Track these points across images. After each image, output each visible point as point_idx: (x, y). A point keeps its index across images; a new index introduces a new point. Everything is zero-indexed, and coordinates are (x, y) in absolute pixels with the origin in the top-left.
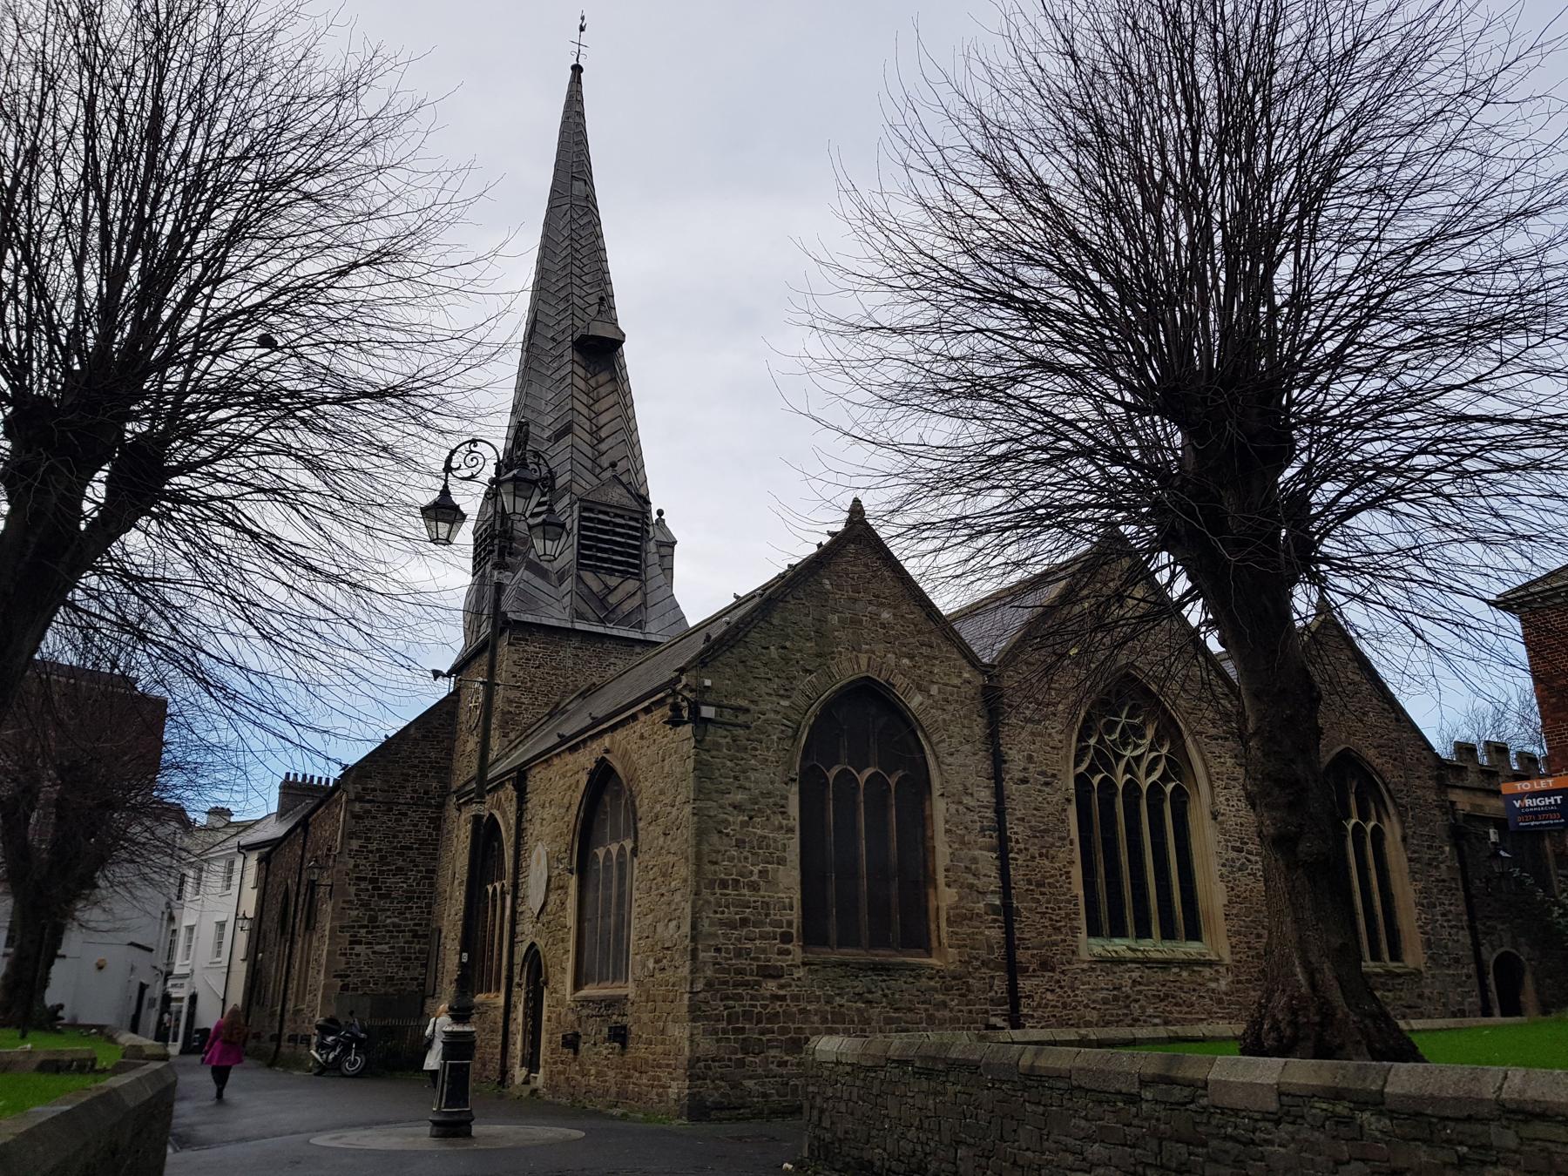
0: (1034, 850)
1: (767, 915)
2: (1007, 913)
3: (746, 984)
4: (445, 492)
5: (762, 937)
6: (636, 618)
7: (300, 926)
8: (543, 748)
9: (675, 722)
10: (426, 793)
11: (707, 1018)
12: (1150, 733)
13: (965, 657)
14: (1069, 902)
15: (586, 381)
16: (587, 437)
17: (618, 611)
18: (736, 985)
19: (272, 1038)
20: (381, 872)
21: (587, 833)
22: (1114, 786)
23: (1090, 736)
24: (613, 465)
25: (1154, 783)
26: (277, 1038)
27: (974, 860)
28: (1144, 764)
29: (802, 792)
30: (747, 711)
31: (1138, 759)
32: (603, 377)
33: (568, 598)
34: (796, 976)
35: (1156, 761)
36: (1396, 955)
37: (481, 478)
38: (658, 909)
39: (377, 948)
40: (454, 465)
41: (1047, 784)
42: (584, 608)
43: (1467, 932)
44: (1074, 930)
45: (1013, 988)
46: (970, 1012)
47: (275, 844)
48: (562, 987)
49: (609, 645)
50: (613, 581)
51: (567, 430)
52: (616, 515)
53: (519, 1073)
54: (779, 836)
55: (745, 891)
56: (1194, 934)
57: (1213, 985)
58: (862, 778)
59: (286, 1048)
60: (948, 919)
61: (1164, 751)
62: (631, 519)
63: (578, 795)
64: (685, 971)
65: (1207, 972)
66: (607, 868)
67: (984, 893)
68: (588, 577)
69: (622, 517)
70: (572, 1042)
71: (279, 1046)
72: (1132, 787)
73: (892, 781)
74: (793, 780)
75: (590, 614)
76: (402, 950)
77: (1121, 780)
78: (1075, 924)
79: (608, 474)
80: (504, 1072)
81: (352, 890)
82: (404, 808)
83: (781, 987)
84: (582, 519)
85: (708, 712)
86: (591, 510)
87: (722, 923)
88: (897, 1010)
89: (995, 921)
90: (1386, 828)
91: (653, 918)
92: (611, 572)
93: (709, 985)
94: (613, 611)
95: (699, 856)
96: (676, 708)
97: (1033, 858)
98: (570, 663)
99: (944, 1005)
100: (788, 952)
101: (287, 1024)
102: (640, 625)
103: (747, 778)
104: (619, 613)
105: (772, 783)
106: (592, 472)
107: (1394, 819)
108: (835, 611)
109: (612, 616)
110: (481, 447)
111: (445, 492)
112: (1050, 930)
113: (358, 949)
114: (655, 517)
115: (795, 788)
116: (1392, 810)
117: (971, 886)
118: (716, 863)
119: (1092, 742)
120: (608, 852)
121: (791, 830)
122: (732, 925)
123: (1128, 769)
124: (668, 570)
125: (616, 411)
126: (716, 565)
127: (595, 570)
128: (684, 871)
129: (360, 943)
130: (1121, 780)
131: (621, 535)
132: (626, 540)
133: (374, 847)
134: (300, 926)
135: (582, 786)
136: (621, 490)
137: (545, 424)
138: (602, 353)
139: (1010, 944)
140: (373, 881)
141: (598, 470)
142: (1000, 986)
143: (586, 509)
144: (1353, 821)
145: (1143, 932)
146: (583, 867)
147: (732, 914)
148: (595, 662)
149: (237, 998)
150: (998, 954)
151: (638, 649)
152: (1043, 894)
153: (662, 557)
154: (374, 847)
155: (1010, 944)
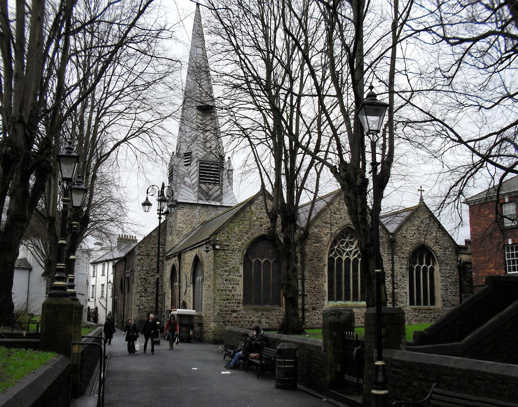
3: (228, 314)
4: (147, 199)
5: (233, 303)
6: (219, 198)
12: (356, 243)
18: (225, 314)
19: (121, 322)
20: (147, 276)
21: (194, 274)
22: (342, 259)
23: (335, 246)
25: (355, 258)
28: (353, 253)
30: (229, 246)
31: (350, 252)
33: (196, 193)
36: (433, 303)
41: (319, 261)
43: (459, 297)
44: (324, 300)
49: (210, 208)
50: (211, 186)
54: (238, 278)
55: (228, 292)
63: (192, 263)
64: (212, 311)
68: (203, 186)
72: (348, 260)
73: (271, 262)
77: (344, 257)
79: (208, 150)
81: (139, 281)
82: (152, 257)
85: (217, 247)
86: (203, 164)
87: (222, 300)
92: (210, 184)
94: (211, 196)
97: (313, 281)
98: (197, 214)
102: (220, 200)
104: (213, 197)
105: (236, 264)
108: (255, 216)
113: (142, 298)
115: (242, 265)
119: (336, 247)
121: (240, 276)
123: (347, 254)
127: (204, 183)
130: (344, 257)
131: (213, 171)
133: (144, 269)
136: (213, 156)
140: (145, 279)
143: (201, 163)
144: (424, 266)
145: (347, 299)
146: (194, 282)
147: (224, 297)
148: (205, 213)
149: (110, 309)
151: (219, 208)
154: (144, 269)
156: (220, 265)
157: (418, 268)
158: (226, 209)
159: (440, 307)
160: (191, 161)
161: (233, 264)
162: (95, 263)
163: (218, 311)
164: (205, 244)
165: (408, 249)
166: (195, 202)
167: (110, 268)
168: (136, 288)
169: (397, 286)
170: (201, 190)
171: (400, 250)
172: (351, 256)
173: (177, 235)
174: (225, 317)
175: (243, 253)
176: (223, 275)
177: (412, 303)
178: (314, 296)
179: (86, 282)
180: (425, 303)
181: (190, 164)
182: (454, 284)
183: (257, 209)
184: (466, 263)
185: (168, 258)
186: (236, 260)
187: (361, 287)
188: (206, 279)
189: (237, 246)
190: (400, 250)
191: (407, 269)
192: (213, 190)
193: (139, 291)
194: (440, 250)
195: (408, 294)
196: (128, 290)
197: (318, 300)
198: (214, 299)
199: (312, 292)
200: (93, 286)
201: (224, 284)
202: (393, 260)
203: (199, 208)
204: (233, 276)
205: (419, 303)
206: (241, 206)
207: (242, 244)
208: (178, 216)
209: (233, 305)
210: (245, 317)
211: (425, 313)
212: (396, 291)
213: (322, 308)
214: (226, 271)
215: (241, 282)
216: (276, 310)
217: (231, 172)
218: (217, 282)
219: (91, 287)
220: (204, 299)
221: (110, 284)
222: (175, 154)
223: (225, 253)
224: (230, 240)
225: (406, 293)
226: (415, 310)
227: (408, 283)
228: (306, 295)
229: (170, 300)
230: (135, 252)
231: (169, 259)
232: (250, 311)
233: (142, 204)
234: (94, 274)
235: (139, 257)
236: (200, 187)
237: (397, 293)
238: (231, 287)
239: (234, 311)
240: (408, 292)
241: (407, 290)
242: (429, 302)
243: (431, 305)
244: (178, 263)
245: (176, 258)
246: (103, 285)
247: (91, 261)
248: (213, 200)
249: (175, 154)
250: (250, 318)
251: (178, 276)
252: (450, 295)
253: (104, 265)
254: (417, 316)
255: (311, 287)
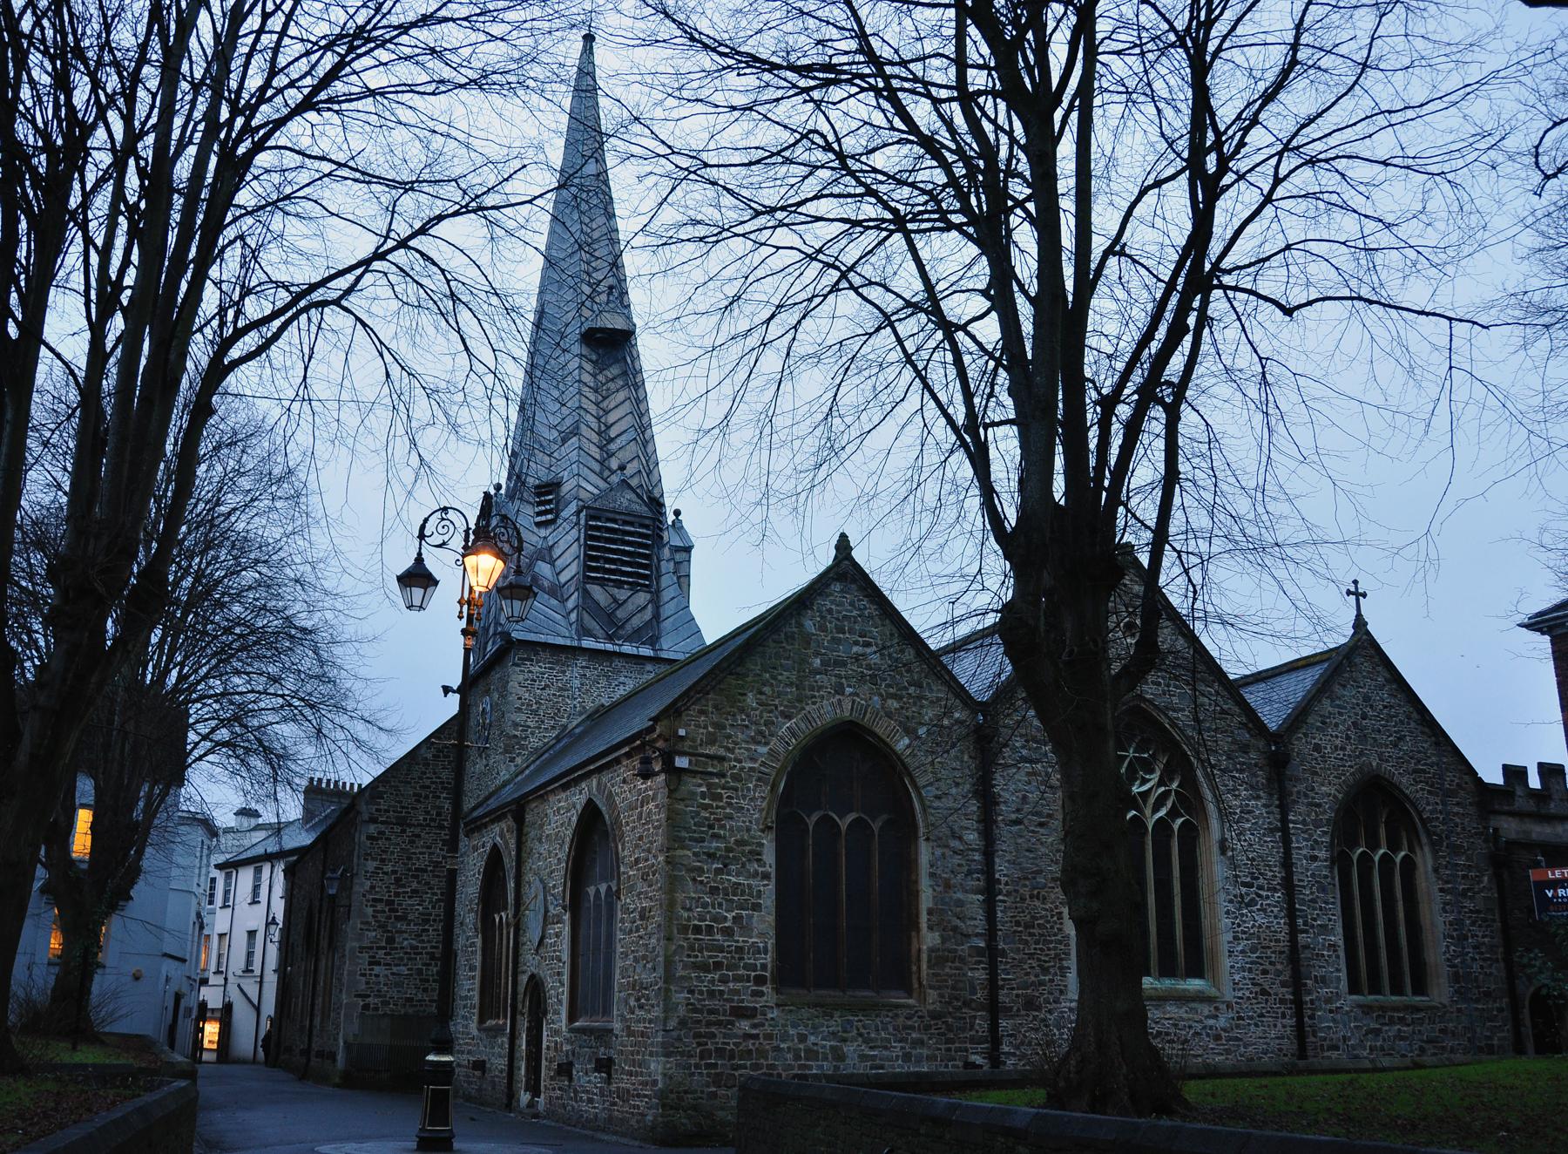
0: (1025, 891)
1: (741, 959)
2: (992, 954)
3: (719, 1023)
4: (419, 559)
5: (737, 979)
6: (650, 633)
7: (324, 943)
8: (543, 780)
9: (646, 775)
10: (439, 814)
11: (682, 1054)
13: (957, 696)
14: (1060, 942)
15: (594, 376)
16: (595, 438)
17: (628, 627)
18: (709, 1024)
20: (397, 894)
21: (579, 872)
24: (622, 468)
26: (306, 1052)
27: (960, 903)
28: (1152, 800)
29: (778, 840)
30: (722, 759)
32: (615, 370)
34: (770, 1016)
35: (1165, 795)
36: (1420, 987)
37: (451, 545)
38: (635, 950)
39: (395, 969)
40: (427, 532)
41: (1041, 825)
42: (590, 622)
43: (1502, 965)
44: (1063, 970)
45: (994, 1026)
46: (949, 1050)
47: (301, 851)
48: (558, 1019)
49: (618, 663)
50: (622, 594)
51: (575, 431)
52: (625, 523)
53: (525, 1097)
55: (719, 937)
56: (1196, 971)
57: (1211, 1022)
58: (844, 824)
59: (314, 1061)
60: (929, 961)
61: (1175, 785)
62: (642, 526)
63: (569, 832)
64: (657, 1012)
65: (1206, 1009)
66: (598, 907)
67: (968, 936)
68: (597, 591)
69: (631, 524)
70: (565, 1070)
71: (309, 1060)
74: (770, 828)
75: (600, 633)
76: (420, 972)
78: (1065, 964)
79: (615, 479)
80: (511, 1095)
81: (370, 911)
82: (417, 831)
83: (754, 1026)
84: (589, 527)
85: (682, 762)
86: (598, 519)
87: (696, 966)
88: (871, 1048)
89: (979, 962)
90: (1419, 860)
91: (660, 943)
92: (619, 584)
93: (682, 1023)
95: (671, 904)
96: (646, 761)
98: (577, 683)
99: (921, 1043)
100: (762, 994)
101: (315, 1039)
102: (653, 641)
103: (723, 827)
105: (748, 830)
106: (600, 475)
107: (1426, 849)
108: (817, 654)
109: (621, 632)
110: (451, 515)
111: (419, 559)
112: (1038, 970)
113: (377, 969)
114: (671, 518)
115: (772, 835)
116: (1424, 840)
117: (955, 929)
118: (690, 909)
120: (598, 891)
121: (766, 876)
122: (704, 968)
124: (683, 580)
125: (627, 407)
126: (725, 594)
127: (601, 582)
128: (657, 918)
129: (379, 964)
132: (637, 542)
133: (389, 868)
134: (324, 943)
135: (574, 825)
136: (630, 495)
137: (550, 419)
138: (612, 346)
139: (993, 985)
140: (390, 903)
141: (606, 473)
142: (981, 1025)
146: (576, 904)
148: (603, 682)
149: (269, 1008)
150: (980, 995)
151: (649, 667)
152: (1031, 935)
153: (677, 563)
154: (389, 868)
155: (993, 985)
156: (688, 830)
157: (1365, 859)
158: (664, 668)
159: (1446, 1001)
160: (557, 512)
161: (739, 829)
162: (230, 867)
163: (682, 1011)
164: (628, 755)
165: (1328, 791)
166: (568, 643)
167: (275, 880)
168: (358, 933)
169: (1305, 923)
170: (587, 601)
171: (1306, 796)
172: (1148, 812)
173: (506, 751)
174: (706, 1035)
175: (774, 787)
176: (700, 871)
177: (1354, 988)
178: (1031, 956)
179: (193, 917)
180: (1397, 989)
181: (552, 522)
182: (1485, 920)
183: (823, 628)
184: (1513, 844)
185: (477, 826)
186: (751, 812)
187: (1185, 927)
188: (631, 889)
189: (753, 760)
190: (1306, 796)
191: (1333, 863)
192: (630, 607)
193: (366, 943)
194: (1432, 799)
195: (1342, 954)
196: (330, 944)
197: (1045, 971)
198: (669, 964)
199: (1021, 941)
200: (221, 936)
201: (705, 905)
202: (1285, 830)
203: (582, 662)
204: (737, 875)
205: (1375, 989)
206: (739, 640)
207: (772, 754)
208: (513, 685)
209: (738, 986)
210: (785, 1037)
211: (1402, 1020)
212: (1302, 938)
213: (1057, 1001)
214: (711, 856)
215: (768, 901)
216: (898, 1006)
217: (684, 555)
218: (680, 896)
219: (215, 939)
220: (619, 964)
221: (273, 927)
222: (503, 491)
223: (709, 786)
224: (729, 736)
225: (1333, 946)
226: (1367, 1009)
227: (1338, 911)
228: (1003, 953)
229: (478, 973)
230: (359, 813)
231: (479, 829)
232: (805, 1013)
233: (400, 579)
234: (226, 899)
235: (372, 829)
236: (586, 594)
237: (1306, 947)
238: (730, 916)
239: (741, 1013)
240: (1341, 943)
241: (1338, 938)
242: (1408, 980)
243: (1415, 993)
244: (513, 846)
245: (507, 824)
246: (252, 934)
247: (221, 859)
248: (629, 639)
249: (503, 491)
250: (803, 1038)
251: (511, 885)
252: (1473, 959)
253: (258, 871)
254: (1377, 1032)
255: (1018, 924)
